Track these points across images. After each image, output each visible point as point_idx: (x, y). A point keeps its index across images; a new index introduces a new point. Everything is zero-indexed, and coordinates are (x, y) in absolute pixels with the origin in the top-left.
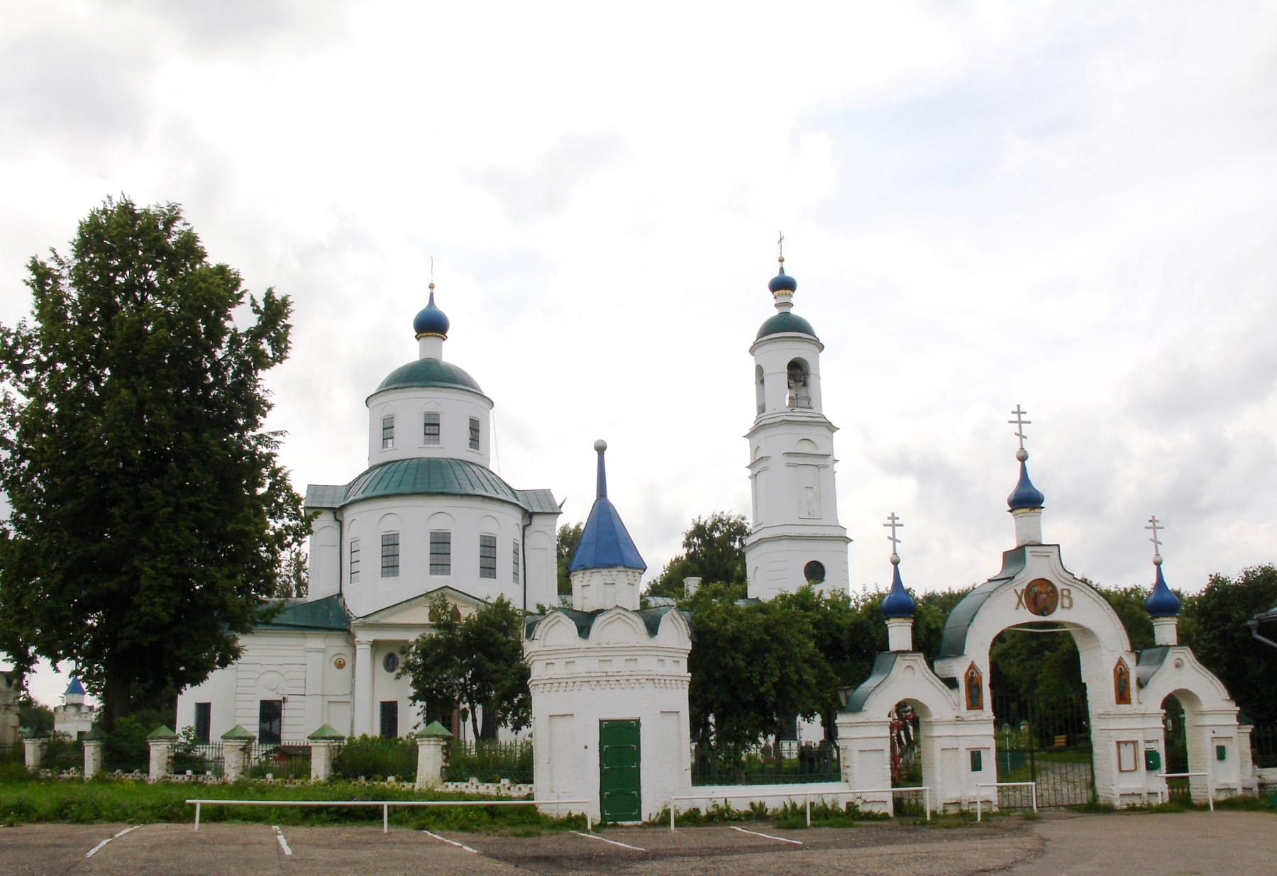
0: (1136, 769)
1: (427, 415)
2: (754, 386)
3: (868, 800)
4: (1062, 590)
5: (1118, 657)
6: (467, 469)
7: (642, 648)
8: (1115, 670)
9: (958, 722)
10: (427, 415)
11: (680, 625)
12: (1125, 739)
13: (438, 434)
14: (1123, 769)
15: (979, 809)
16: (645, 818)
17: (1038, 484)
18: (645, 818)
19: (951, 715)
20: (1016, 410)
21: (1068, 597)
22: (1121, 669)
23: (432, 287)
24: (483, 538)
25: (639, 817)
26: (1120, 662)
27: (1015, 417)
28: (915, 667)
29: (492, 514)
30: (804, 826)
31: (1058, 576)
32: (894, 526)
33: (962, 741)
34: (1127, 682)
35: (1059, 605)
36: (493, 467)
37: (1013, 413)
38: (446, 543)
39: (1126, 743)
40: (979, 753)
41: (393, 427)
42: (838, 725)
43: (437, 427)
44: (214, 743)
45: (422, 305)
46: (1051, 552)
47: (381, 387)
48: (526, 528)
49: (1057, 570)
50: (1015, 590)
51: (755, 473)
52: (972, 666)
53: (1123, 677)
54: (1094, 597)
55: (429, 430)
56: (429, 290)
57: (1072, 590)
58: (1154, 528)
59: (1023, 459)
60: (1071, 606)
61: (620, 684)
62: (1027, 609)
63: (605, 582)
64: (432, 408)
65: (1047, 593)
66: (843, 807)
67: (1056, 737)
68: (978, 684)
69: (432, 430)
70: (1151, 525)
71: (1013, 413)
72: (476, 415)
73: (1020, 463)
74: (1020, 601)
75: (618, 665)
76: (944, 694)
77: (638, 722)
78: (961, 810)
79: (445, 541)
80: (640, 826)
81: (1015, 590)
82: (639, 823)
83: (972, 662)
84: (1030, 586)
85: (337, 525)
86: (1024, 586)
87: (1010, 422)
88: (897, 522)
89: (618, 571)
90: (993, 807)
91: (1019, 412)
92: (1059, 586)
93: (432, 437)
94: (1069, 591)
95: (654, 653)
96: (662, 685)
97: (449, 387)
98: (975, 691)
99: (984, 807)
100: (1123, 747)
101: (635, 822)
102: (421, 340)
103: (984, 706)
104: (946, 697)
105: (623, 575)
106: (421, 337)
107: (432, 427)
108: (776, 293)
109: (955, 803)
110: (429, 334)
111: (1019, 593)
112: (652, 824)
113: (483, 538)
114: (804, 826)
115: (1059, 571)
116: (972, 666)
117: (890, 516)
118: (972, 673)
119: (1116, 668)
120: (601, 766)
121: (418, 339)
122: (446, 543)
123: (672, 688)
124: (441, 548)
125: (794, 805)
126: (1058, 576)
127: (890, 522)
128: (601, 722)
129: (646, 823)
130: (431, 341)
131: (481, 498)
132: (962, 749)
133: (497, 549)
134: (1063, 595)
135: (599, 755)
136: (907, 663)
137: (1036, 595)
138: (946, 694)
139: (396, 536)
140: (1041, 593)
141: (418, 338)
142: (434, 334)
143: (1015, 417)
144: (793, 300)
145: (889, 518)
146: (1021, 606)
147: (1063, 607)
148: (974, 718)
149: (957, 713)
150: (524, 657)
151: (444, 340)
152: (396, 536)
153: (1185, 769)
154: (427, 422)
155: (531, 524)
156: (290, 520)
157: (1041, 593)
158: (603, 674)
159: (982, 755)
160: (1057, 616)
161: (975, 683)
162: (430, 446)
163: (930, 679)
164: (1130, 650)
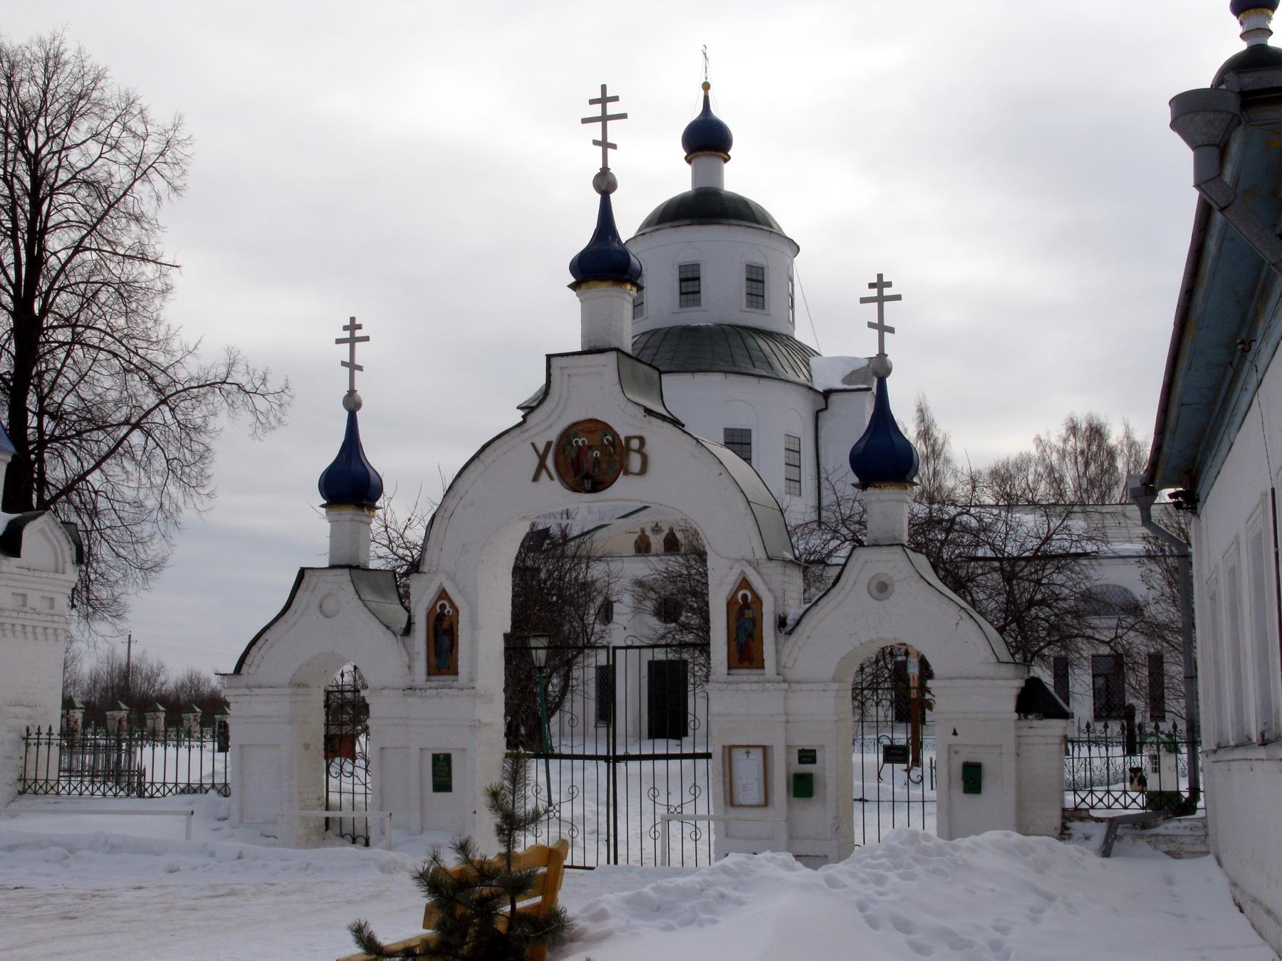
1: (683, 268)
4: (628, 439)
10: (683, 268)
20: (609, 95)
21: (640, 451)
22: (745, 596)
26: (745, 583)
32: (352, 341)
34: (757, 622)
37: (592, 102)
38: (746, 444)
39: (748, 748)
40: (447, 758)
43: (697, 282)
44: (45, 730)
45: (695, 112)
47: (639, 230)
48: (821, 415)
53: (749, 614)
55: (687, 287)
58: (881, 299)
60: (643, 471)
64: (687, 257)
65: (602, 447)
67: (909, 725)
69: (690, 286)
70: (874, 293)
71: (592, 102)
72: (758, 260)
74: (542, 466)
79: (744, 442)
83: (443, 594)
84: (568, 435)
86: (553, 435)
87: (585, 121)
88: (358, 333)
93: (691, 297)
94: (642, 440)
97: (756, 228)
98: (446, 641)
102: (693, 162)
103: (460, 670)
107: (690, 283)
108: (1242, 15)
116: (443, 594)
117: (357, 322)
118: (443, 607)
122: (746, 444)
127: (347, 334)
130: (705, 160)
139: (696, 267)
140: (590, 448)
141: (689, 160)
143: (596, 110)
144: (1272, 26)
145: (345, 328)
146: (544, 475)
150: (643, 602)
152: (696, 267)
154: (684, 276)
155: (826, 408)
157: (590, 448)
161: (446, 625)
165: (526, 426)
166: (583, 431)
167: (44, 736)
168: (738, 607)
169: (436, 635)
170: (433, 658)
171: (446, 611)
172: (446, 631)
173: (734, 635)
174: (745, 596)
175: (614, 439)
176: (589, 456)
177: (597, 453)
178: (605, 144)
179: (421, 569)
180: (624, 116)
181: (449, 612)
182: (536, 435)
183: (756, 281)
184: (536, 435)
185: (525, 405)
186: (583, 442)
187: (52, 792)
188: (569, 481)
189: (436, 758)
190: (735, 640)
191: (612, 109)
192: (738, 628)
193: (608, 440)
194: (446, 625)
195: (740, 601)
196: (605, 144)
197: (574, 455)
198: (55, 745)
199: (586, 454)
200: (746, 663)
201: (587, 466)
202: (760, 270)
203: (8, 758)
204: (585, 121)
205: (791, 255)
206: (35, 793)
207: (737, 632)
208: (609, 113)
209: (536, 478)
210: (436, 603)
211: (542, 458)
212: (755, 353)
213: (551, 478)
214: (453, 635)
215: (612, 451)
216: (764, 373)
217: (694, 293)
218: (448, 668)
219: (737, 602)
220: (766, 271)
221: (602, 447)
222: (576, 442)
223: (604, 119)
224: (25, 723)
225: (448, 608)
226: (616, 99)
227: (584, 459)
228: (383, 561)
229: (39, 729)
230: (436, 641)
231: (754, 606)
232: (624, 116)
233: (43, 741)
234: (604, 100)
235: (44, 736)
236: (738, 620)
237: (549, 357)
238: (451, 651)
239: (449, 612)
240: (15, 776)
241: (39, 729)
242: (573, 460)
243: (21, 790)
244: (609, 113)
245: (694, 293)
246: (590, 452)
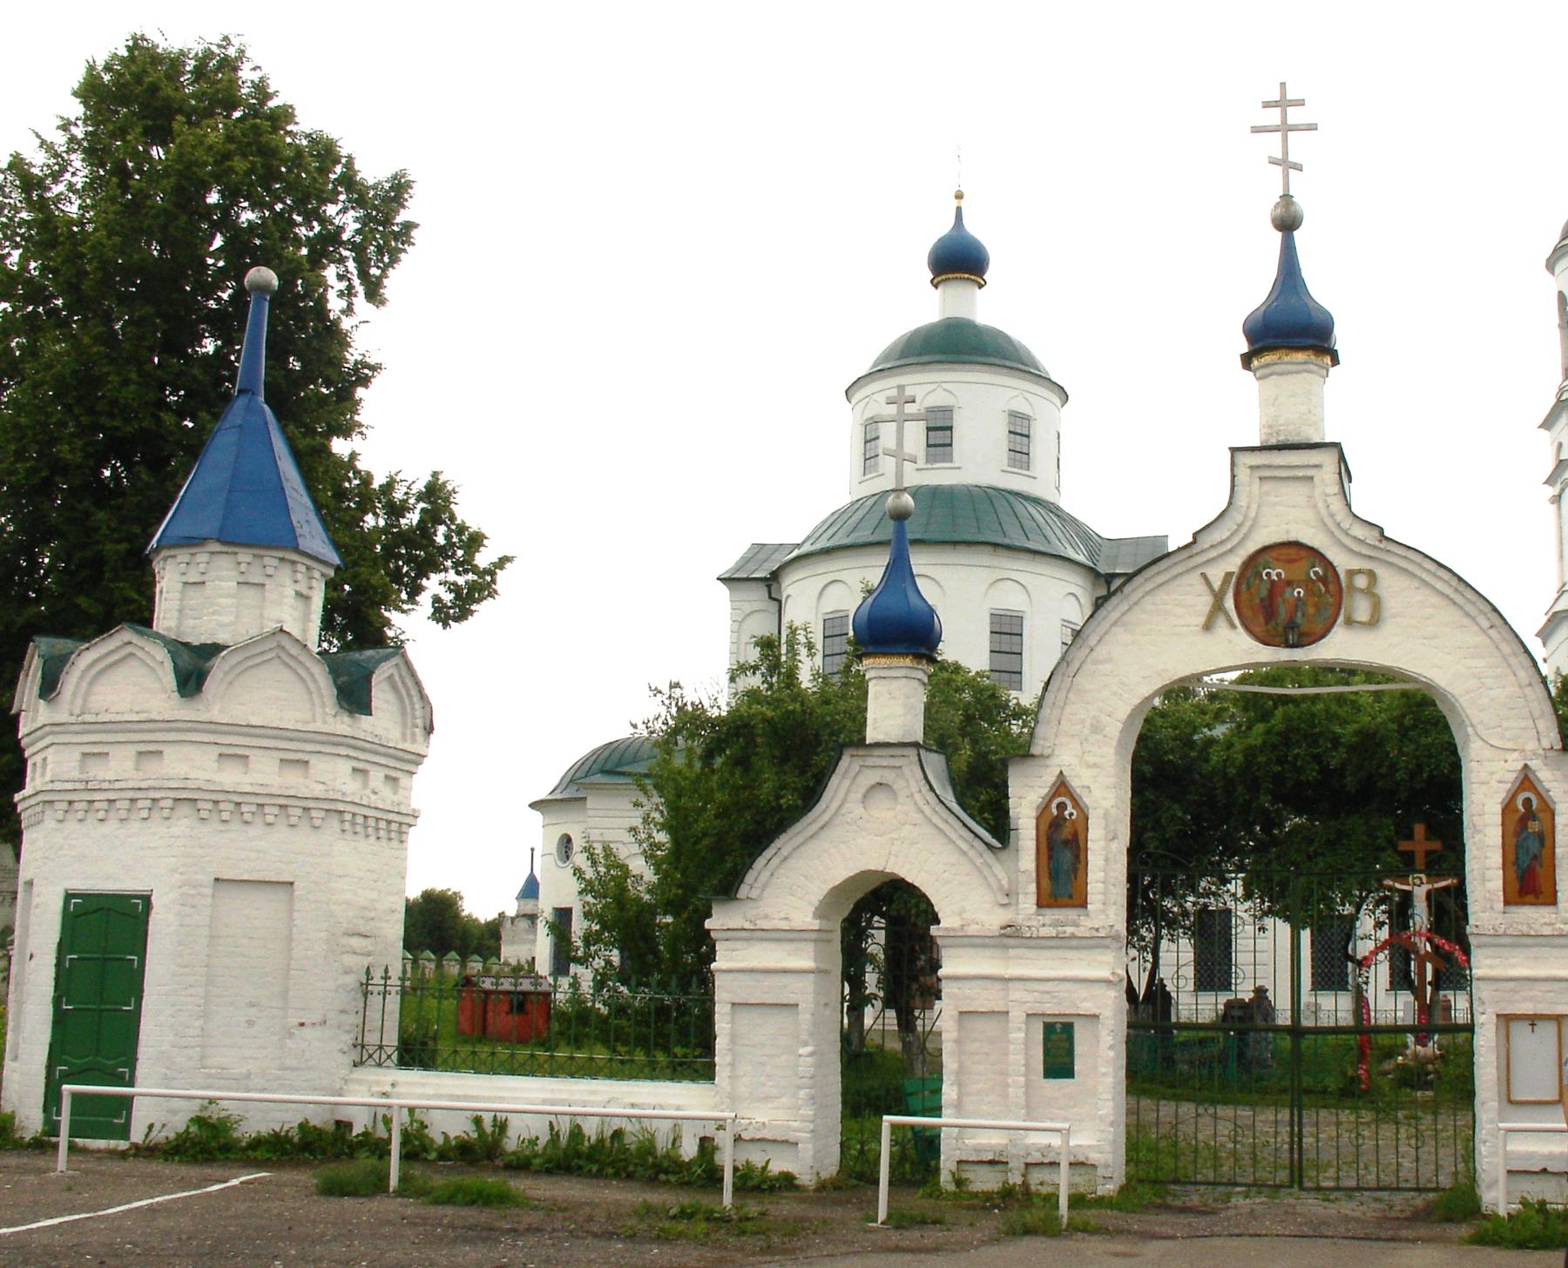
0: (1511, 1102)
2: (1558, 330)
3: (745, 1136)
4: (1351, 573)
5: (1519, 766)
6: (1019, 508)
7: (169, 725)
8: (1508, 808)
9: (1005, 940)
11: (312, 675)
12: (1527, 1008)
13: (951, 445)
14: (1516, 1097)
15: (1063, 1183)
16: (137, 1135)
17: (1322, 288)
18: (137, 1135)
19: (993, 920)
22: (1527, 802)
23: (959, 196)
24: (996, 617)
25: (124, 1132)
26: (1526, 780)
27: (1273, 118)
28: (899, 785)
29: (1013, 575)
30: (379, 1185)
31: (1337, 533)
33: (1017, 993)
35: (1341, 619)
36: (1068, 503)
37: (1267, 105)
39: (1533, 1020)
40: (1068, 1028)
41: (878, 438)
42: (939, 941)
45: (944, 227)
46: (1316, 466)
47: (875, 365)
49: (1332, 516)
50: (1204, 575)
51: (1556, 492)
52: (1061, 786)
53: (1534, 826)
54: (1449, 591)
56: (955, 203)
57: (1380, 571)
59: (1287, 223)
61: (288, 816)
62: (1240, 629)
63: (185, 579)
65: (1308, 583)
66: (689, 1150)
68: (1075, 835)
69: (938, 437)
71: (1267, 105)
73: (1279, 235)
74: (1218, 607)
75: (120, 767)
76: (973, 863)
77: (147, 900)
78: (1005, 1182)
80: (123, 1155)
81: (1204, 575)
82: (123, 1145)
85: (773, 606)
86: (1234, 564)
87: (1256, 130)
89: (212, 553)
90: (1100, 1181)
91: (1283, 103)
92: (1342, 562)
94: (1372, 575)
95: (212, 738)
96: (382, 833)
98: (1067, 856)
99: (1077, 1179)
100: (1520, 1031)
101: (113, 1143)
104: (980, 872)
105: (286, 570)
106: (939, 283)
109: (991, 1163)
110: (951, 276)
111: (1217, 585)
112: (147, 1151)
113: (996, 617)
114: (379, 1185)
115: (1339, 518)
116: (1061, 786)
118: (1062, 806)
119: (1512, 798)
120: (57, 1002)
121: (936, 286)
123: (390, 839)
124: (1006, 643)
125: (576, 1133)
126: (1337, 533)
128: (69, 896)
129: (135, 1146)
131: (989, 549)
132: (1017, 1016)
133: (1025, 638)
134: (1351, 586)
135: (53, 975)
136: (872, 777)
137: (1274, 588)
138: (979, 861)
140: (1290, 583)
142: (958, 275)
147: (1350, 622)
148: (1052, 932)
149: (1003, 916)
151: (981, 286)
152: (947, 411)
153: (936, 1111)
156: (458, 573)
157: (1290, 583)
158: (78, 786)
159: (1077, 1036)
160: (1339, 646)
161: (1066, 833)
162: (937, 465)
163: (935, 819)
164: (1559, 746)
165: (1196, 549)
166: (1277, 559)
167: (377, 980)
168: (1517, 817)
169: (1050, 849)
170: (1046, 882)
171: (1066, 813)
172: (1066, 843)
173: (1512, 857)
174: (1527, 802)
175: (1325, 571)
176: (1287, 595)
177: (1299, 591)
178: (1286, 164)
179: (1035, 750)
180: (1312, 127)
181: (1071, 814)
182: (1209, 561)
183: (1020, 433)
184: (1209, 561)
185: (727, 576)
186: (1279, 575)
187: (371, 1062)
188: (1257, 629)
189: (1049, 1029)
190: (1514, 864)
191: (1295, 116)
192: (1517, 847)
193: (1316, 573)
194: (1066, 833)
195: (1521, 807)
196: (1286, 164)
197: (1264, 593)
198: (393, 993)
199: (1283, 593)
200: (1530, 898)
201: (1283, 612)
202: (1026, 418)
203: (343, 1012)
204: (1256, 130)
205: (1059, 404)
206: (379, 1065)
207: (1517, 854)
208: (1290, 121)
209: (1208, 626)
210: (1050, 801)
211: (1218, 598)
212: (1028, 523)
213: (1233, 626)
214: (1078, 847)
215: (1323, 589)
216: (1042, 548)
217: (945, 445)
218: (1071, 897)
219: (1517, 810)
220: (1032, 423)
221: (1308, 583)
222: (1268, 574)
223: (1285, 128)
224: (366, 961)
225: (1070, 809)
226: (1300, 103)
227: (1280, 599)
228: (321, 787)
229: (386, 971)
230: (1050, 857)
231: (1541, 815)
232: (1312, 127)
233: (376, 989)
234: (1283, 103)
235: (377, 980)
236: (1517, 834)
237: (1233, 450)
238: (1075, 871)
239: (1071, 814)
240: (348, 1039)
241: (386, 971)
242: (1262, 600)
243: (357, 1059)
244: (1290, 121)
245: (945, 445)
246: (1288, 590)
